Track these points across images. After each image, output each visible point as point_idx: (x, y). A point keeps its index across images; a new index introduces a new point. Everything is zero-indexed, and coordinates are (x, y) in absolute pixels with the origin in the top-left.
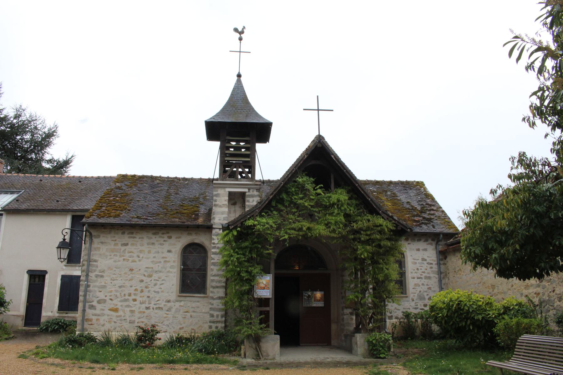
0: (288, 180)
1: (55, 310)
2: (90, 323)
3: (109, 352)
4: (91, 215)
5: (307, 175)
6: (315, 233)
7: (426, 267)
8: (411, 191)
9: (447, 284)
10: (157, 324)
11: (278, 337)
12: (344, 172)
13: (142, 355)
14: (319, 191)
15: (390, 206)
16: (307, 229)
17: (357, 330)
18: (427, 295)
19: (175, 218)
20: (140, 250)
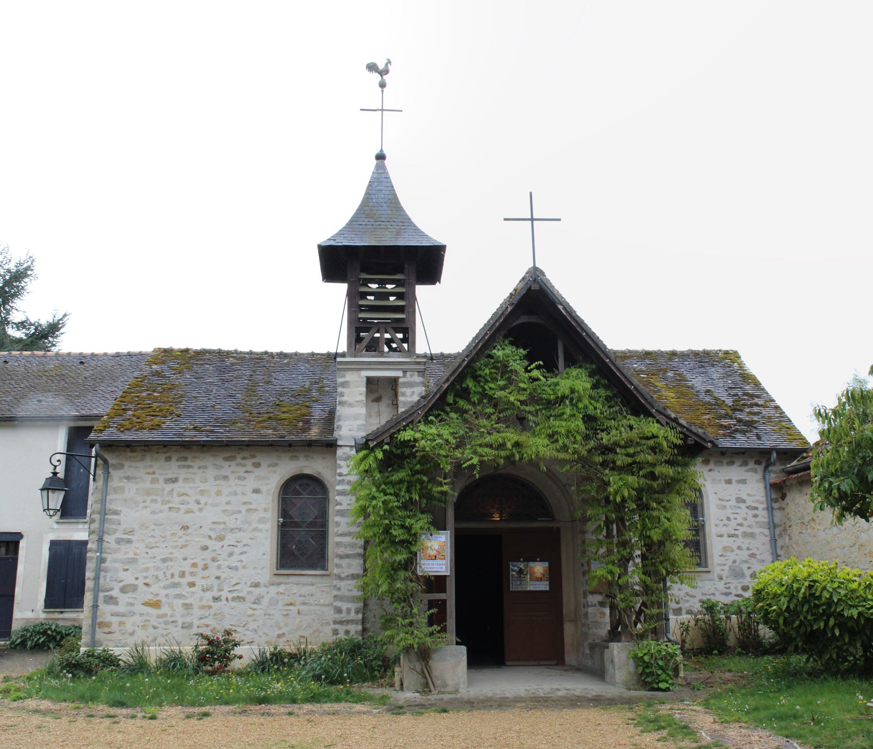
0: (477, 354)
1: (38, 607)
2: (107, 630)
3: (143, 684)
4: (105, 427)
5: (512, 343)
6: (530, 453)
7: (745, 515)
8: (713, 369)
9: (788, 547)
10: (234, 628)
11: (463, 649)
12: (582, 336)
13: (207, 689)
14: (536, 373)
15: (673, 398)
16: (513, 447)
17: (614, 635)
18: (749, 568)
19: (266, 428)
20: (201, 490)
